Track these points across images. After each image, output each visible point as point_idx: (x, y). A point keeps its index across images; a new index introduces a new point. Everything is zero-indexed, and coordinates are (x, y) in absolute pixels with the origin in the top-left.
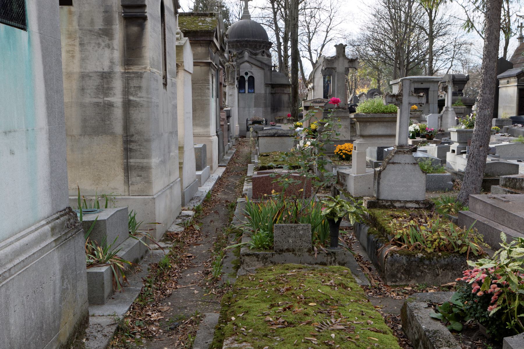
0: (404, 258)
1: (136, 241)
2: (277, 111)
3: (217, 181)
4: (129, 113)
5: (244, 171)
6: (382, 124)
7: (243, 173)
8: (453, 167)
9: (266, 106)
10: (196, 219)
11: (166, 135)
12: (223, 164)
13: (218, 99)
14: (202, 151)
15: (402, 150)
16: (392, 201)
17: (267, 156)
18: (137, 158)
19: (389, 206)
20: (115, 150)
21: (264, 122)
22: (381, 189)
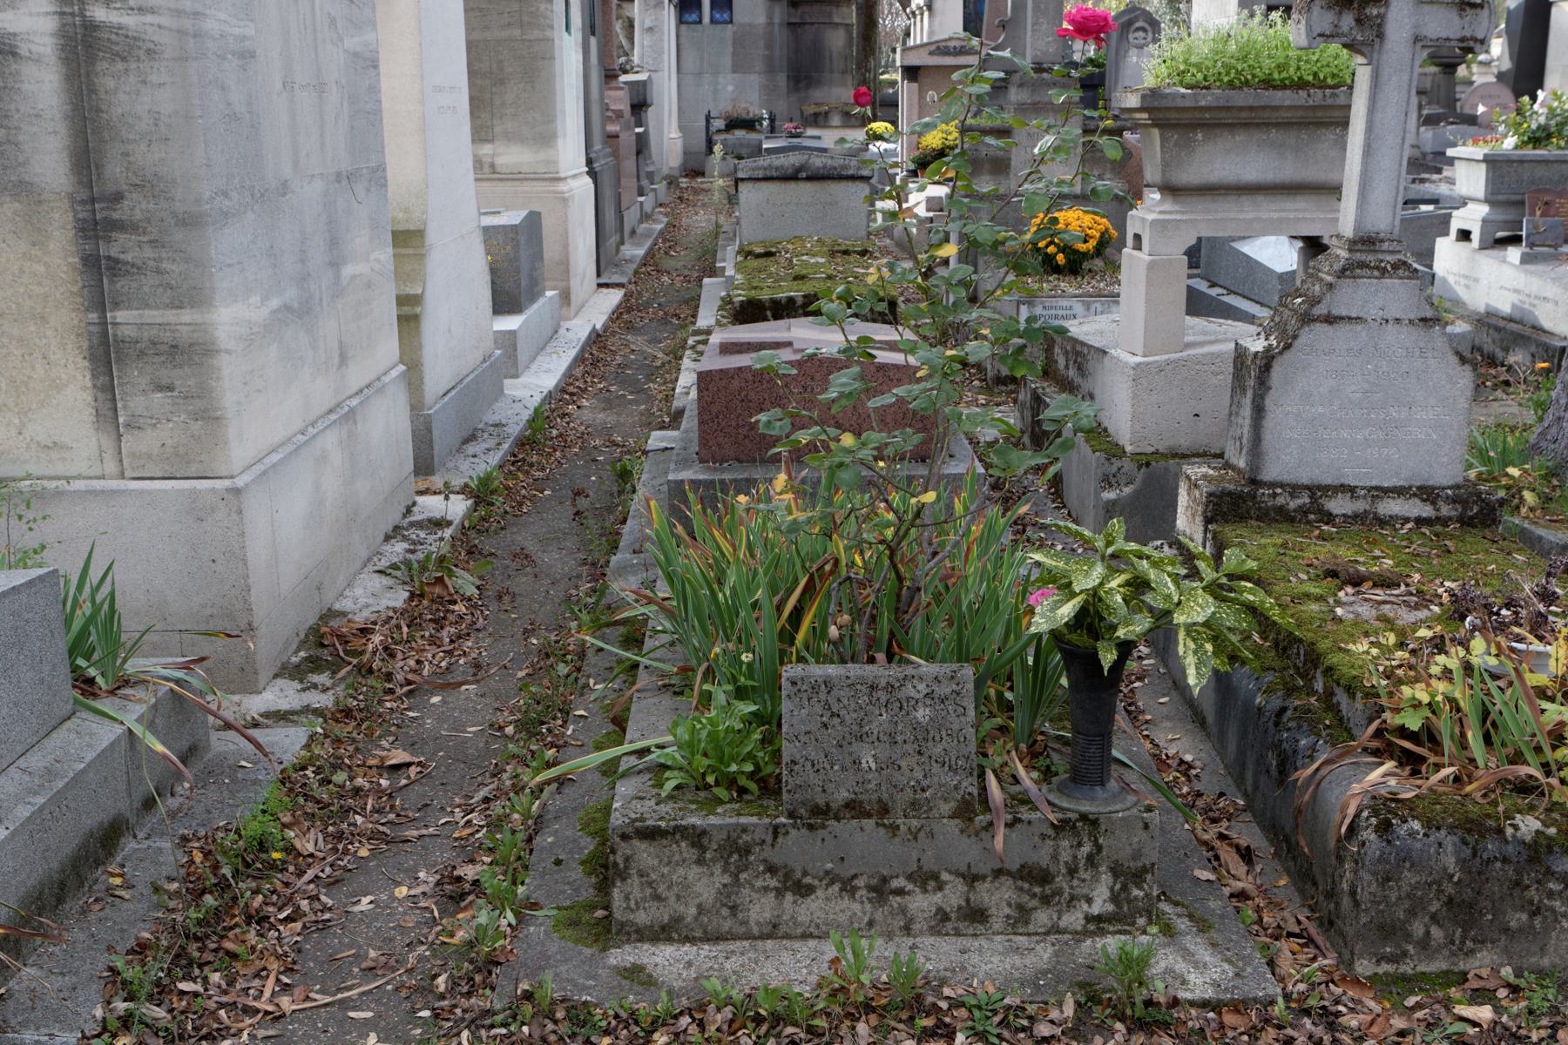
0: (1450, 842)
1: (107, 734)
2: (808, 86)
3: (582, 350)
4: (93, 91)
5: (686, 302)
6: (1259, 135)
7: (685, 312)
8: (1463, 294)
9: (770, 70)
10: (470, 542)
11: (310, 192)
12: (616, 279)
13: (593, 41)
14: (522, 239)
15: (1370, 258)
16: (1318, 491)
17: (768, 254)
18: (147, 306)
19: (1303, 511)
20: (41, 269)
21: (765, 123)
22: (1267, 436)
